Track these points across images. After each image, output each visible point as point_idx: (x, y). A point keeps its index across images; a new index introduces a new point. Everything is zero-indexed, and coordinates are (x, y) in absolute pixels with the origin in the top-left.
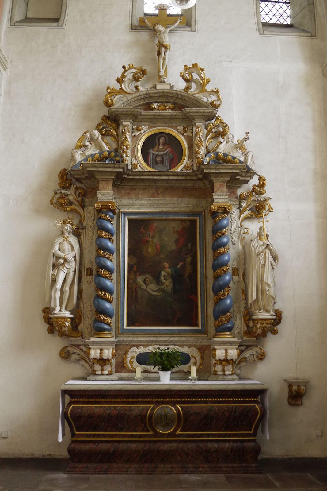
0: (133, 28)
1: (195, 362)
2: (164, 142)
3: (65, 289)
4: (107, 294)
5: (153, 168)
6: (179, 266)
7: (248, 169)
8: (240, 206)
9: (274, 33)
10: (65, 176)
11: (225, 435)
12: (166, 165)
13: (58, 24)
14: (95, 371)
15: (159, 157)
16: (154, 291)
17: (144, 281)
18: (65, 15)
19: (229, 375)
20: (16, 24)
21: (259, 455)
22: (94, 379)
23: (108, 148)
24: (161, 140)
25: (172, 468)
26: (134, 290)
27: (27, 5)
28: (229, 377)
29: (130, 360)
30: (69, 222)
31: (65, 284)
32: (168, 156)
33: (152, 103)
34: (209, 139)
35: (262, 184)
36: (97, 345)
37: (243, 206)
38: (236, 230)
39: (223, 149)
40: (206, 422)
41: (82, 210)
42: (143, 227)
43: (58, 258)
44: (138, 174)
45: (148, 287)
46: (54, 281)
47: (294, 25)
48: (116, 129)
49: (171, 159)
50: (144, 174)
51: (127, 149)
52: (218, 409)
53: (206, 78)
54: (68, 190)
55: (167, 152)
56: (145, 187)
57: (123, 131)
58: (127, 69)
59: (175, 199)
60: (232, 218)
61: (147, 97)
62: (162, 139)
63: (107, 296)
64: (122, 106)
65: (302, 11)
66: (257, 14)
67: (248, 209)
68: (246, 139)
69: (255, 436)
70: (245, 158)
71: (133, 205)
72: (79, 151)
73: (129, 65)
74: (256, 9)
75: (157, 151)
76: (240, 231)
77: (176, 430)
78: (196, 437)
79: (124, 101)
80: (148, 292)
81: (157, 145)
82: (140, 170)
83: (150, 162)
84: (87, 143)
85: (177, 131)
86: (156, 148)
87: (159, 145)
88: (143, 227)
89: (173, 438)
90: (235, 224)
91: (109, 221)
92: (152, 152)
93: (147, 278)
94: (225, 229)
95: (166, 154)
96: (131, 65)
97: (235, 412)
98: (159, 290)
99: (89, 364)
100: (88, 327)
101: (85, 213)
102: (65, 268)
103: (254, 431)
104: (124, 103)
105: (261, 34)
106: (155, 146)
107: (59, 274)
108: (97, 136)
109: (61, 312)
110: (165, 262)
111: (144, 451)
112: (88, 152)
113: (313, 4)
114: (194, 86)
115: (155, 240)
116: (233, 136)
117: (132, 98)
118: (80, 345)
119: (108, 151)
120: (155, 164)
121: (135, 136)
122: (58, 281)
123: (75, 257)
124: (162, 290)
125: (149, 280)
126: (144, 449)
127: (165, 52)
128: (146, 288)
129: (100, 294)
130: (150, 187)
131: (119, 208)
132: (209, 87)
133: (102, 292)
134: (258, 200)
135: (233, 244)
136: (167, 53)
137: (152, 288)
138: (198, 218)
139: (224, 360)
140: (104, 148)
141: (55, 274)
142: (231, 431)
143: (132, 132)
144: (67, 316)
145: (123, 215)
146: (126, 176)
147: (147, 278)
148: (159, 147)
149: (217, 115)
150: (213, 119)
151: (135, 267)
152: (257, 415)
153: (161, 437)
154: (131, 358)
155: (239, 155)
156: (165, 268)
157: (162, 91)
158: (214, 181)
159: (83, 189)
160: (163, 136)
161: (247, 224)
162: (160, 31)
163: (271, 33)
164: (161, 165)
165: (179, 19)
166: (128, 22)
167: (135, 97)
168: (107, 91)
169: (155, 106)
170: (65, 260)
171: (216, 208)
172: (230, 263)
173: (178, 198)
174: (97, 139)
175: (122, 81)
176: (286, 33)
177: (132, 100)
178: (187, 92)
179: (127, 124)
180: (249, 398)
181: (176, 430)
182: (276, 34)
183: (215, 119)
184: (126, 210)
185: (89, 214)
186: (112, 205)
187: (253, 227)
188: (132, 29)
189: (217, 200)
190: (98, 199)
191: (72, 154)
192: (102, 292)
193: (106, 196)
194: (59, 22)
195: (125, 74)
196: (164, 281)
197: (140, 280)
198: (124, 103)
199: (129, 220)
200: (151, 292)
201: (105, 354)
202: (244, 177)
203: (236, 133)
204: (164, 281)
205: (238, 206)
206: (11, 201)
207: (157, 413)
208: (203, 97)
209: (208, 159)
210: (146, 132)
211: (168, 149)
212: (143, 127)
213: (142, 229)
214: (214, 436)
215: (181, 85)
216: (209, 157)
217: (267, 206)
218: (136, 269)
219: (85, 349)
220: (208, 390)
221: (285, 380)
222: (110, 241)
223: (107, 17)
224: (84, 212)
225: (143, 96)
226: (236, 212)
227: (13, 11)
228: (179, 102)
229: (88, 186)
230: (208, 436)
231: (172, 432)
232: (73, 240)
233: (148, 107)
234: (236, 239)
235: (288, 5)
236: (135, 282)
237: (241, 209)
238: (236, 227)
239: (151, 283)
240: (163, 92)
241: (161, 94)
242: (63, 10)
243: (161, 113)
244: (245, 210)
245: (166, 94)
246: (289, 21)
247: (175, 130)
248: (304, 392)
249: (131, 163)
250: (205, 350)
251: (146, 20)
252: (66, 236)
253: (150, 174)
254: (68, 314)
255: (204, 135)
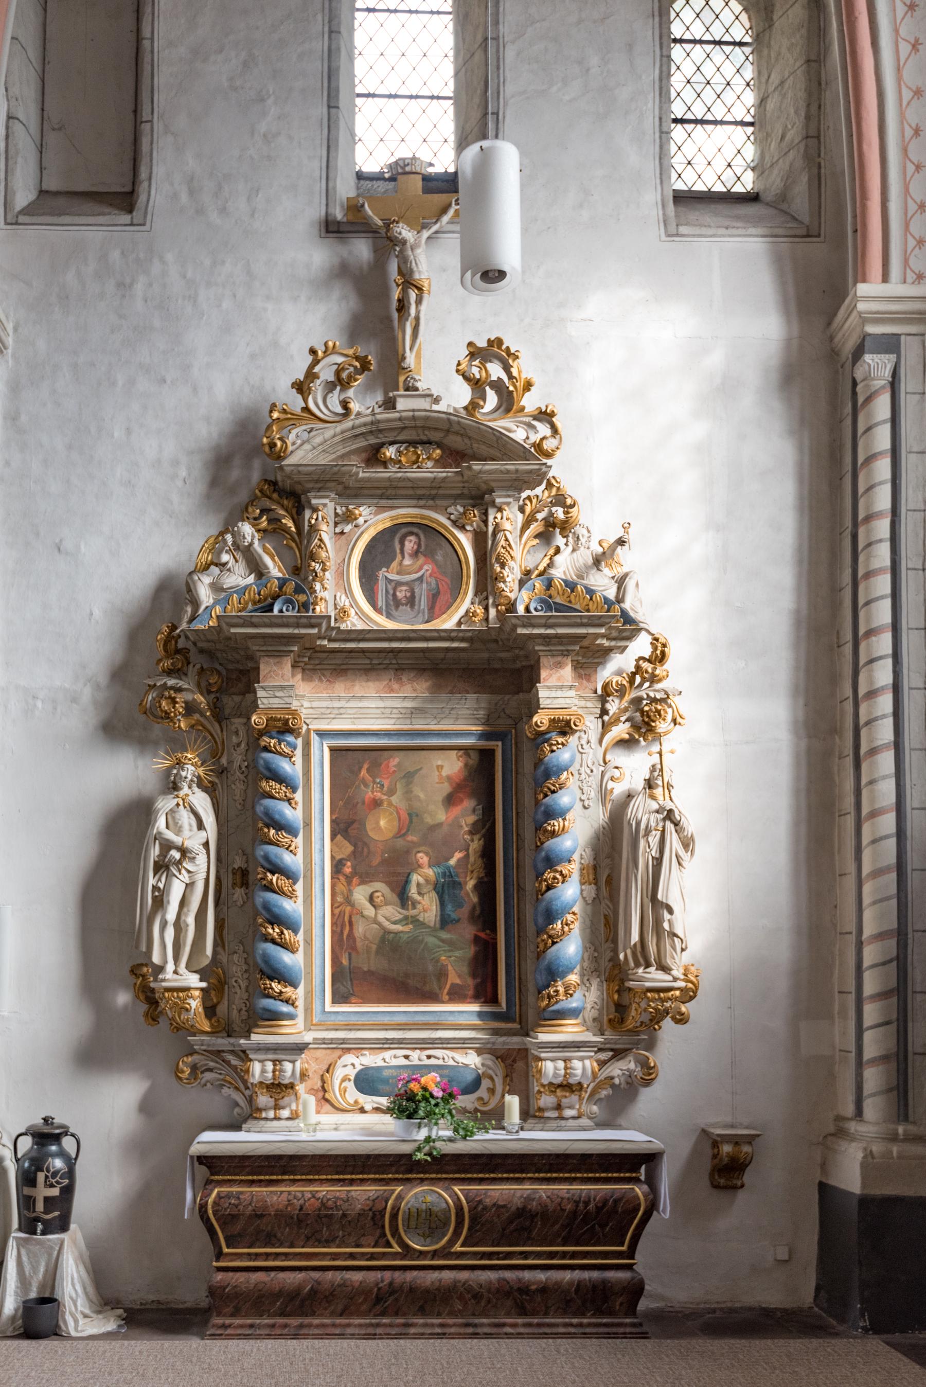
0: (331, 229)
1: (491, 1086)
2: (415, 547)
3: (185, 921)
4: (285, 932)
5: (389, 616)
6: (452, 862)
7: (626, 618)
8: (604, 712)
9: (704, 231)
10: (173, 642)
11: (564, 1255)
12: (422, 607)
13: (132, 218)
14: (260, 1110)
15: (404, 588)
16: (395, 923)
17: (371, 899)
18: (149, 192)
19: (574, 1118)
20: (22, 219)
21: (641, 1302)
22: (259, 1130)
23: (276, 570)
24: (407, 543)
25: (442, 1325)
26: (346, 919)
27: (41, 153)
28: (571, 1123)
29: (341, 1084)
30: (190, 760)
31: (185, 910)
32: (424, 586)
33: (382, 445)
34: (528, 539)
35: (659, 656)
36: (266, 1054)
37: (611, 713)
38: (592, 771)
39: (565, 566)
40: (522, 1224)
41: (217, 725)
42: (366, 766)
43: (167, 846)
44: (353, 636)
45: (380, 912)
46: (160, 902)
47: (762, 196)
48: (296, 517)
49: (434, 592)
50: (367, 636)
51: (324, 570)
52: (548, 1197)
53: (524, 376)
54: (183, 677)
55: (423, 576)
56: (369, 667)
57: (313, 521)
58: (320, 354)
59: (444, 696)
60: (584, 742)
61: (371, 432)
62: (411, 541)
63: (287, 937)
64: (310, 456)
65: (785, 154)
66: (661, 174)
67: (623, 719)
68: (621, 542)
69: (633, 1259)
70: (619, 588)
71: (339, 714)
72: (205, 576)
73: (326, 344)
74: (660, 158)
75: (398, 573)
76: (603, 774)
77: (452, 1242)
78: (498, 1259)
79: (315, 445)
80: (379, 924)
81: (399, 557)
82: (360, 626)
83: (381, 602)
84: (225, 557)
85: (449, 518)
86: (394, 565)
87: (403, 557)
88: (366, 766)
89: (444, 1260)
90: (590, 757)
91: (286, 757)
92: (386, 574)
93: (377, 891)
94: (565, 773)
95: (420, 579)
96: (331, 344)
97: (587, 1203)
98: (405, 920)
99: (244, 1095)
100: (241, 1010)
101: (225, 733)
102: (183, 871)
103: (629, 1247)
104: (314, 448)
105: (669, 236)
106: (393, 560)
107: (170, 886)
108: (249, 539)
109: (179, 977)
110: (419, 852)
111: (379, 1289)
112: (227, 581)
113: (818, 137)
114: (492, 399)
115: (394, 799)
116: (589, 532)
117: (335, 436)
118: (223, 1051)
119: (278, 579)
120: (393, 608)
121: (342, 533)
122: (168, 902)
123: (206, 845)
124: (415, 921)
125: (383, 896)
126: (381, 1285)
127: (419, 301)
128: (376, 915)
129: (270, 934)
130: (381, 667)
131: (308, 721)
132: (530, 402)
133: (273, 929)
134: (648, 695)
135: (585, 808)
136: (423, 308)
137: (389, 915)
138: (500, 743)
139: (560, 1086)
140: (267, 568)
141: (161, 885)
142: (575, 1246)
143: (336, 524)
144: (193, 985)
145: (317, 738)
146: (325, 642)
147: (377, 891)
148: (402, 561)
149: (550, 475)
150: (539, 485)
151: (349, 864)
152: (639, 1210)
153: (417, 1259)
154: (343, 1080)
155: (603, 583)
156: (420, 866)
157: (411, 414)
158: (541, 653)
159: (219, 672)
160: (412, 533)
161: (619, 758)
162: (404, 242)
163: (697, 231)
164: (408, 608)
165: (453, 203)
166: (317, 212)
167: (343, 432)
168: (271, 417)
169: (390, 452)
170: (184, 851)
171: (546, 722)
172: (576, 857)
173: (451, 692)
174: (251, 544)
175: (309, 389)
176: (738, 228)
177: (335, 439)
178: (473, 416)
179: (326, 508)
180: (619, 1171)
181: (452, 1242)
182: (710, 232)
183: (543, 486)
184: (324, 726)
185: (234, 737)
186: (294, 718)
187: (633, 767)
188: (328, 231)
189: (549, 701)
190: (259, 702)
191: (188, 584)
192: (273, 929)
193: (278, 694)
194: (134, 213)
195: (316, 369)
196: (418, 898)
197: (360, 894)
198: (314, 448)
199: (333, 750)
200: (386, 924)
201: (284, 1072)
202: (614, 639)
203: (597, 523)
204: (418, 898)
205: (598, 711)
206: (39, 704)
207: (409, 1206)
208: (515, 428)
209: (525, 595)
210: (372, 521)
211: (426, 567)
212: (361, 509)
213: (364, 772)
214: (538, 1255)
215: (456, 396)
216: (528, 590)
217: (670, 711)
218: (350, 870)
219: (235, 1062)
220: (524, 1155)
221: (704, 1131)
222: (290, 804)
223: (260, 196)
224: (222, 731)
225: (363, 430)
226: (592, 727)
227: (9, 179)
228: (454, 441)
229: (231, 667)
230: (525, 1255)
231: (444, 1248)
232: (201, 801)
233: (374, 457)
234: (593, 794)
235: (750, 130)
236: (348, 901)
237: (606, 718)
238: (593, 764)
239: (386, 904)
240: (414, 418)
241: (407, 423)
242: (143, 175)
243: (409, 475)
244: (616, 721)
245: (419, 423)
246: (747, 183)
247: (442, 515)
248: (749, 1158)
249: (335, 605)
250: (514, 1061)
251: (366, 205)
252: (182, 793)
253: (383, 635)
254: (193, 981)
255: (515, 528)
